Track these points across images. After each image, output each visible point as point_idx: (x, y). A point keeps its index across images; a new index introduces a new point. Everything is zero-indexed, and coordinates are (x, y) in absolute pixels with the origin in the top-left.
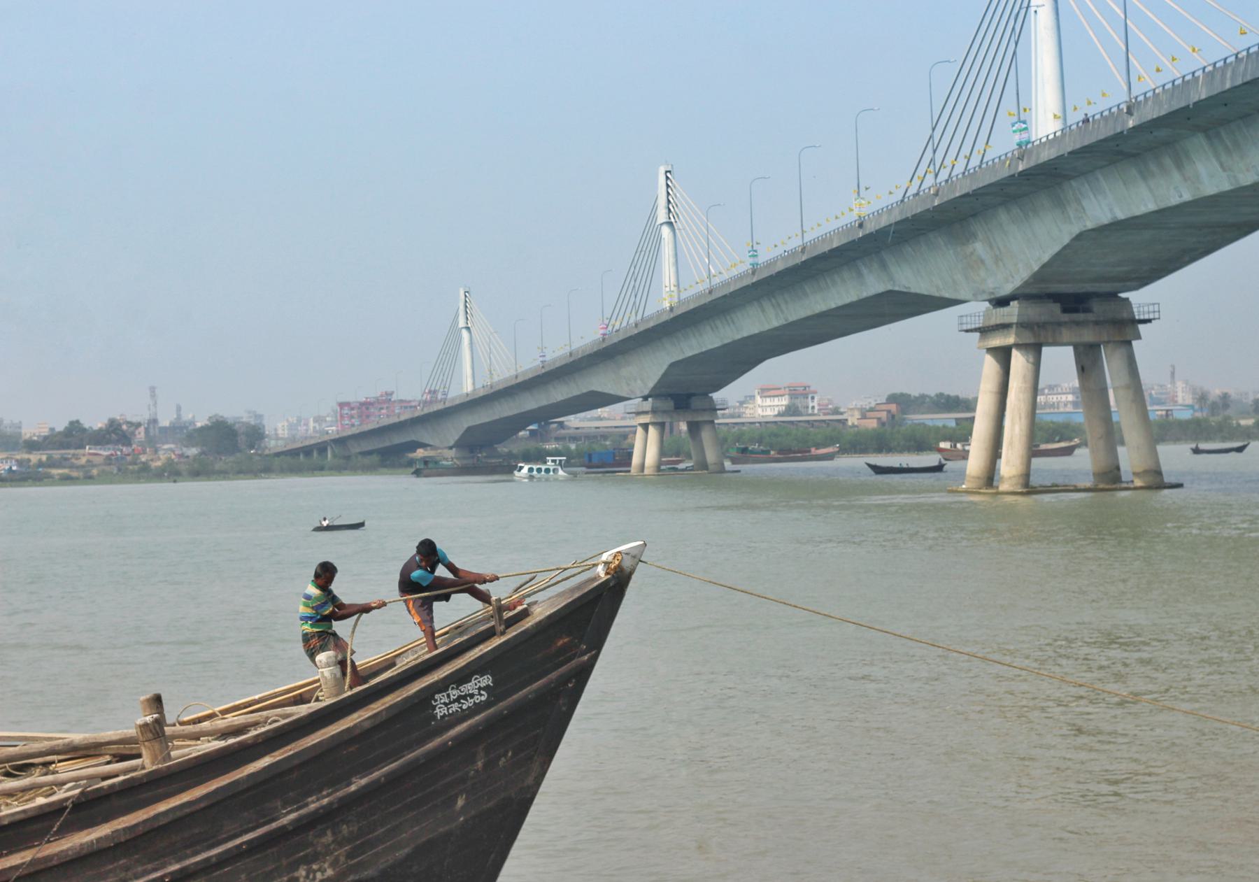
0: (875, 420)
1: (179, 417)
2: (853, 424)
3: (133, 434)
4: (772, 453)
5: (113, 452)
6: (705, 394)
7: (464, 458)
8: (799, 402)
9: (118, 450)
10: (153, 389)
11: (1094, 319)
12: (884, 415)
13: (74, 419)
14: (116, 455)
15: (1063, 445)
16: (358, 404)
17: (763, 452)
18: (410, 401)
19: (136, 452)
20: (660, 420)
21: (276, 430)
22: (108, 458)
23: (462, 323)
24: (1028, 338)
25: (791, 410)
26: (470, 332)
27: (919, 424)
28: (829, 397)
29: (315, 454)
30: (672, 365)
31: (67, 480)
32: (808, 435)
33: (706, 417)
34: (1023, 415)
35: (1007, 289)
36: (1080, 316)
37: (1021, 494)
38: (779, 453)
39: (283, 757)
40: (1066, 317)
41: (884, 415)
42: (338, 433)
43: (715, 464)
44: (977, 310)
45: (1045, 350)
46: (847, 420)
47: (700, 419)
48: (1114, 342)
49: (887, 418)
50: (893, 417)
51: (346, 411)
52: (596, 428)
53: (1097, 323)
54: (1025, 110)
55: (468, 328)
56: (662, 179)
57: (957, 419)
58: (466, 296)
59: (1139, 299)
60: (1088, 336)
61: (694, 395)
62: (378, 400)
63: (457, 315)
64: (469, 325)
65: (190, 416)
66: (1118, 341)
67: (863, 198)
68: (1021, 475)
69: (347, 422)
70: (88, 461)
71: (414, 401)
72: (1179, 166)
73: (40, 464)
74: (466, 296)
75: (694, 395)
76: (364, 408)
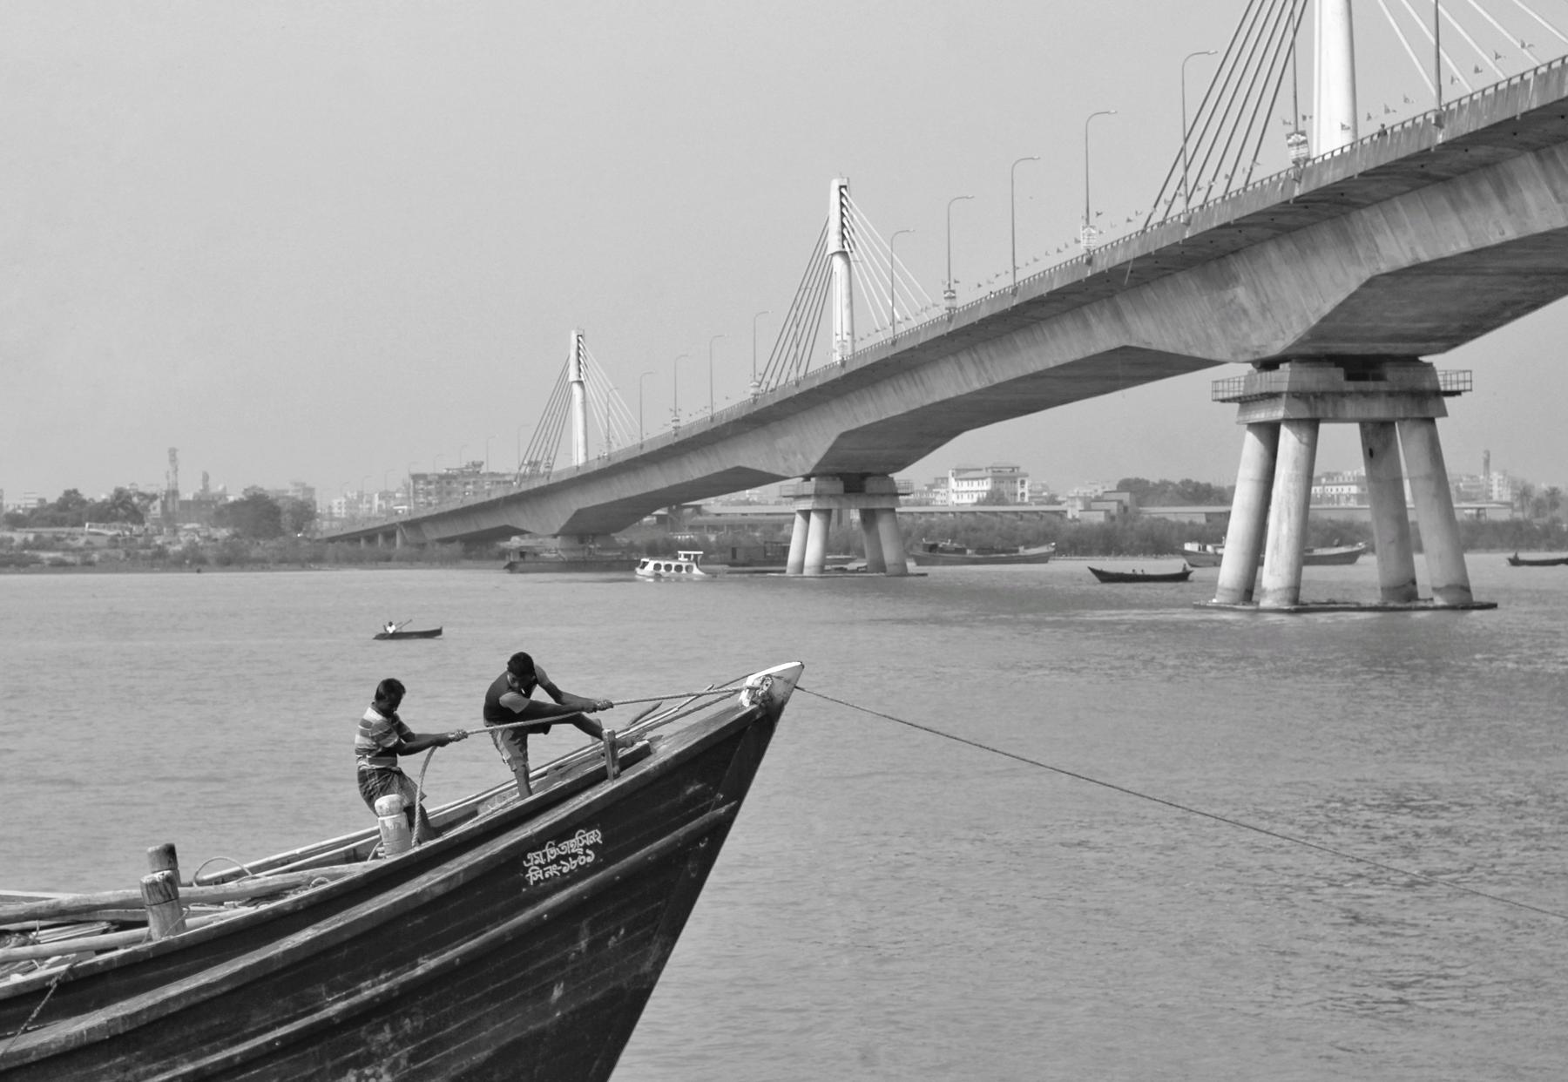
0: (1102, 513)
1: (206, 488)
2: (1074, 517)
3: (146, 508)
4: (969, 551)
5: (120, 532)
6: (884, 475)
7: (572, 550)
8: (1005, 488)
9: (127, 529)
10: (173, 453)
11: (1386, 389)
12: (1113, 507)
13: (71, 488)
14: (124, 535)
15: (1343, 550)
16: (437, 477)
17: (957, 551)
18: (504, 475)
19: (150, 532)
20: (825, 506)
21: (330, 507)
22: (114, 539)
23: (573, 376)
24: (1302, 411)
25: (994, 497)
28: (1044, 482)
29: (380, 539)
30: (843, 436)
31: (59, 566)
33: (884, 504)
34: (1293, 511)
35: (1276, 348)
36: (1370, 385)
37: (1289, 612)
38: (977, 553)
40: (1351, 386)
41: (1113, 507)
43: (895, 564)
44: (1237, 374)
45: (1323, 427)
46: (1066, 512)
47: (877, 506)
49: (1118, 510)
50: (1126, 509)
51: (421, 485)
52: (743, 514)
53: (1390, 394)
54: (1304, 118)
56: (574, 342)
57: (1207, 514)
59: (1445, 364)
60: (1379, 410)
61: (869, 475)
62: (462, 472)
63: (567, 366)
64: (583, 379)
65: (220, 488)
66: (1417, 419)
67: (1093, 227)
69: (422, 500)
70: (88, 542)
71: (509, 474)
73: (26, 545)
74: (579, 341)
75: (869, 475)
76: (444, 482)
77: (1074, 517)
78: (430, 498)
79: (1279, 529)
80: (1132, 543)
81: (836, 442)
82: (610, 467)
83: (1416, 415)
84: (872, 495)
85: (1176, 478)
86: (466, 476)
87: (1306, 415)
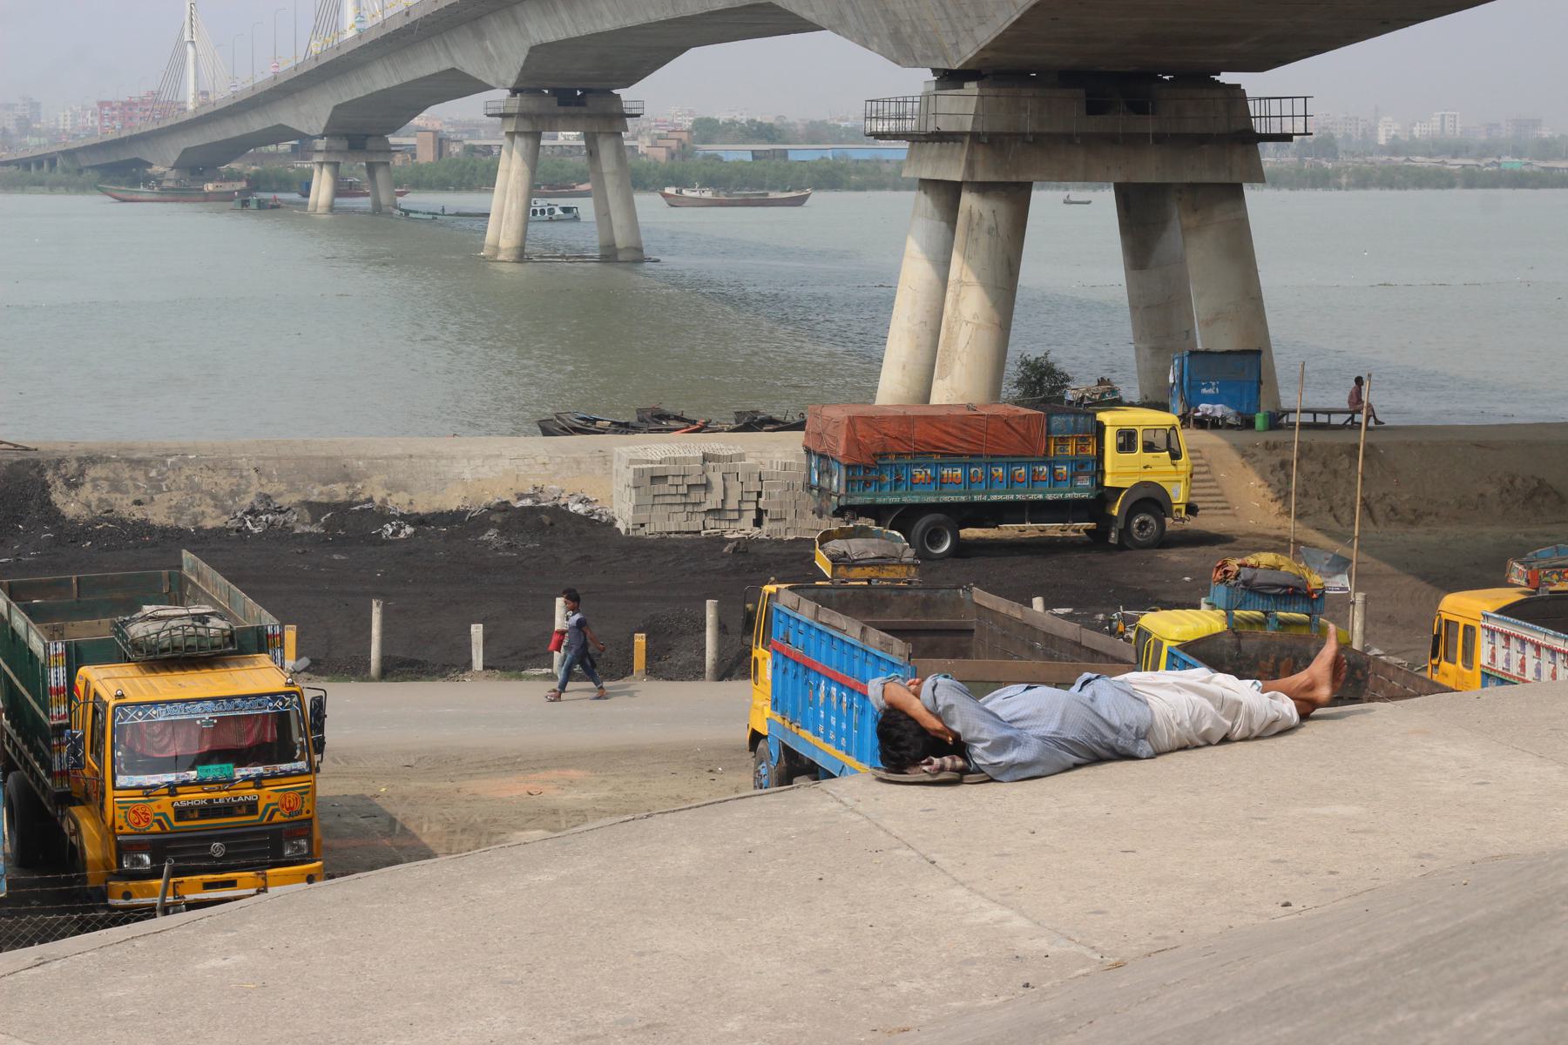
2: (642, 152)
4: (543, 187)
6: (381, 137)
12: (674, 144)
15: (793, 194)
20: (333, 160)
21: (57, 120)
23: (187, 37)
26: (195, 47)
27: (711, 156)
28: (691, 108)
30: (336, 108)
32: (562, 167)
33: (381, 159)
38: (548, 189)
39: (995, 693)
40: (562, 110)
46: (637, 146)
47: (374, 160)
48: (606, 133)
49: (678, 147)
50: (684, 146)
51: (106, 111)
53: (589, 116)
55: (193, 42)
57: (753, 151)
58: (191, 7)
61: (368, 136)
64: (194, 39)
68: (516, 247)
72: (516, 22)
74: (191, 7)
75: (368, 136)
77: (642, 152)
78: (114, 122)
79: (511, 207)
82: (177, 124)
83: (606, 131)
85: (743, 118)
87: (530, 130)
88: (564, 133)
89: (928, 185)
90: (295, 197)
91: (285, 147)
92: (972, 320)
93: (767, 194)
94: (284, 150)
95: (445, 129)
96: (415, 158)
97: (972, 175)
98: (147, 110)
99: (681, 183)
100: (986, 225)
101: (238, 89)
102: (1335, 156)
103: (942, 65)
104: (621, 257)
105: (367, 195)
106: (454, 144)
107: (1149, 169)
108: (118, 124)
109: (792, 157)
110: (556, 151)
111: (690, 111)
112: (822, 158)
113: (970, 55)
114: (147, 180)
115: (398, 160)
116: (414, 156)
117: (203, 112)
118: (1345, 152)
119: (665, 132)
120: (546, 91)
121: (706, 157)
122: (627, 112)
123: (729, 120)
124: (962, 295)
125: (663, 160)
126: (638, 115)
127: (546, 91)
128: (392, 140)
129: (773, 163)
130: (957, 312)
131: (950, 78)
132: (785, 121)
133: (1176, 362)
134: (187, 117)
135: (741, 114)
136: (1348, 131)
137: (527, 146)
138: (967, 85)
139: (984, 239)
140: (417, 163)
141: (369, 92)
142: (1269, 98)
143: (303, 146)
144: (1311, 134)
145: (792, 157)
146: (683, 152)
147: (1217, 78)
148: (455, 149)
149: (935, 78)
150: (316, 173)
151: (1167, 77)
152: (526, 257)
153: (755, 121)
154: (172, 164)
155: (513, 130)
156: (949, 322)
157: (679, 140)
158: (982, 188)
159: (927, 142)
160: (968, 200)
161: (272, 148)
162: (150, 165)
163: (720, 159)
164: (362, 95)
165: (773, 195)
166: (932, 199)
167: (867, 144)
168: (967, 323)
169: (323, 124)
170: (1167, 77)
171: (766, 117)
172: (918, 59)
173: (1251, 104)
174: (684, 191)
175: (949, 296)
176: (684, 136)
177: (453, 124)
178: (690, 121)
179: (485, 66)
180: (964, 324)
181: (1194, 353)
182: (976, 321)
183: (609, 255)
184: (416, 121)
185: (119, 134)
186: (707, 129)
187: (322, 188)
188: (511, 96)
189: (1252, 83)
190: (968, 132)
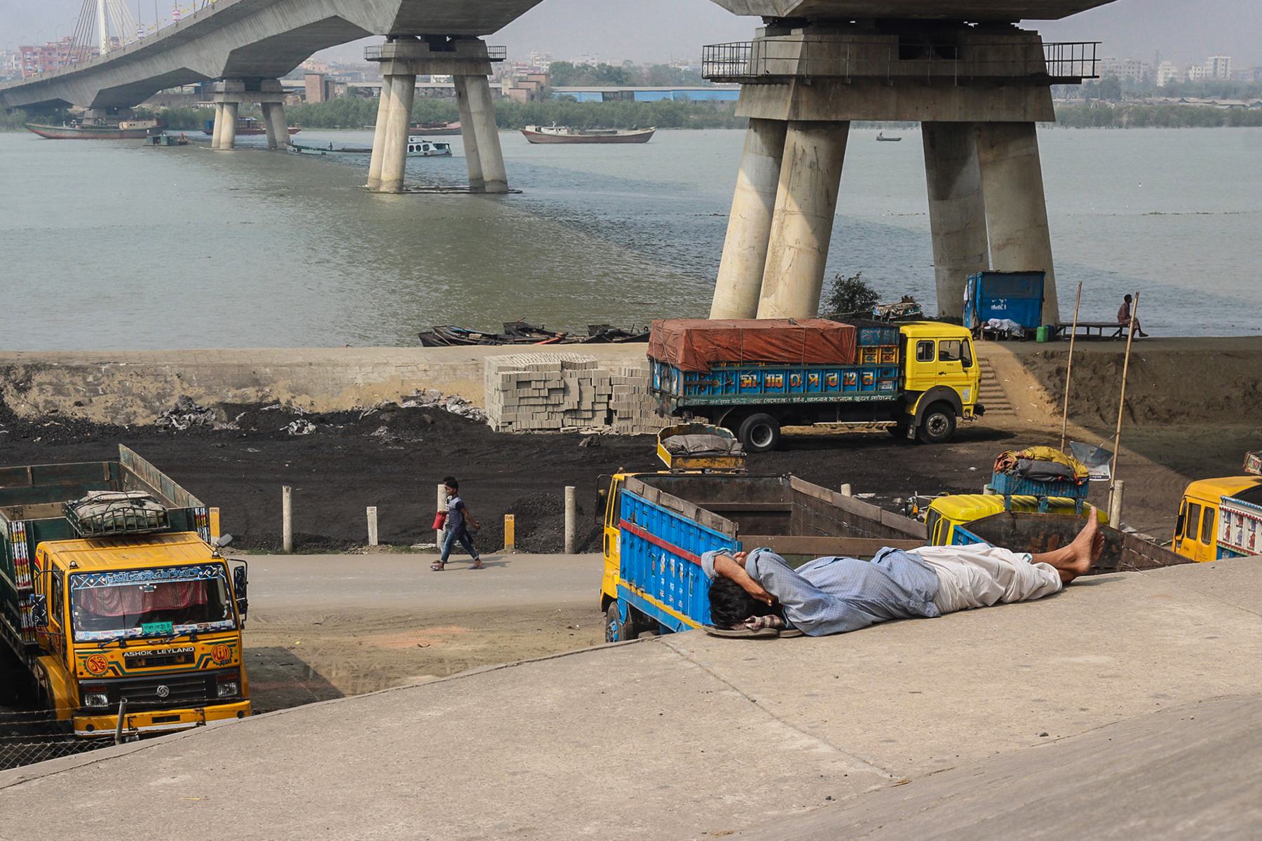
6: (274, 79)
12: (533, 86)
15: (639, 132)
20: (232, 101)
24: (402, 70)
27: (566, 97)
28: (548, 53)
30: (232, 52)
40: (433, 55)
42: (108, 57)
44: (378, 42)
50: (542, 88)
53: (458, 60)
61: (264, 78)
75: (264, 78)
76: (46, 53)
80: (516, 119)
81: (230, 57)
83: (474, 74)
84: (265, 93)
85: (594, 62)
86: (64, 49)
87: (406, 73)
88: (436, 76)
89: (758, 124)
90: (200, 134)
91: (189, 89)
92: (795, 246)
93: (616, 132)
94: (189, 92)
95: (330, 72)
96: (305, 99)
97: (797, 115)
98: (65, 55)
99: (540, 121)
100: (808, 160)
101: (144, 35)
102: (1118, 97)
103: (771, 13)
104: (488, 189)
105: (263, 132)
106: (339, 86)
107: (953, 110)
108: (39, 67)
109: (638, 98)
110: (430, 92)
111: (548, 56)
112: (665, 99)
113: (797, 4)
114: (69, 119)
115: (289, 101)
116: (304, 97)
117: (114, 56)
118: (1127, 93)
119: (526, 75)
120: (419, 38)
121: (562, 98)
122: (491, 56)
123: (582, 64)
124: (786, 223)
125: (524, 101)
126: (501, 60)
127: (419, 38)
128: (284, 82)
129: (621, 103)
130: (781, 238)
131: (778, 26)
132: (632, 65)
133: (970, 282)
134: (101, 61)
135: (593, 59)
136: (1131, 74)
137: (403, 86)
138: (793, 32)
139: (806, 172)
140: (307, 103)
141: (261, 38)
142: (1062, 44)
143: (205, 86)
144: (1098, 77)
145: (638, 98)
146: (541, 94)
147: (1016, 25)
148: (340, 91)
149: (766, 25)
150: (217, 112)
151: (972, 25)
152: (405, 188)
153: (605, 65)
154: (89, 105)
155: (390, 73)
156: (774, 248)
157: (538, 82)
158: (806, 127)
159: (757, 84)
160: (794, 138)
161: (177, 90)
162: (71, 105)
163: (574, 100)
164: (256, 41)
165: (621, 133)
166: (762, 136)
167: (704, 86)
168: (790, 247)
169: (222, 68)
170: (972, 25)
171: (615, 62)
172: (750, 7)
173: (1045, 49)
174: (542, 129)
175: (775, 223)
176: (542, 79)
177: (337, 68)
178: (547, 65)
179: (364, 14)
180: (787, 248)
181: (986, 274)
182: (797, 246)
183: (478, 187)
184: (304, 65)
185: (41, 76)
186: (563, 72)
187: (223, 126)
188: (388, 42)
189: (1047, 30)
190: (794, 75)
